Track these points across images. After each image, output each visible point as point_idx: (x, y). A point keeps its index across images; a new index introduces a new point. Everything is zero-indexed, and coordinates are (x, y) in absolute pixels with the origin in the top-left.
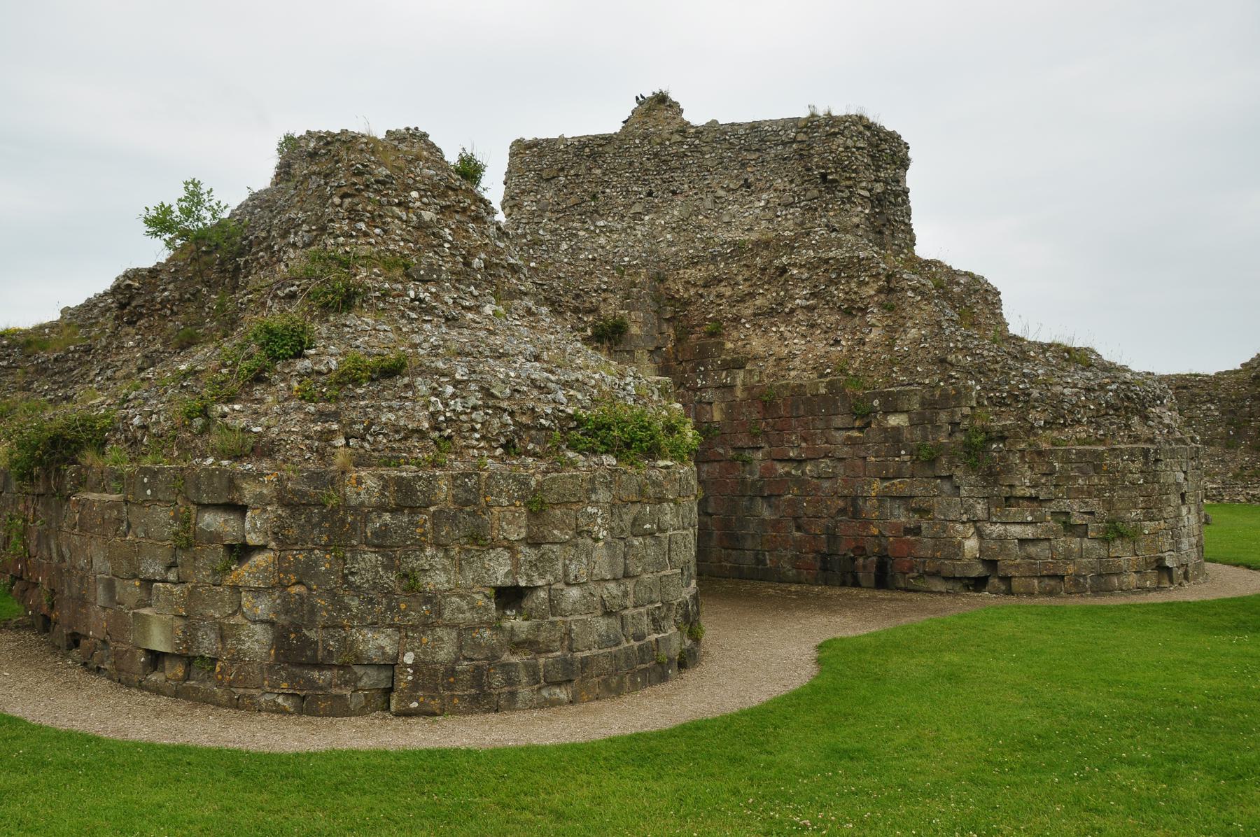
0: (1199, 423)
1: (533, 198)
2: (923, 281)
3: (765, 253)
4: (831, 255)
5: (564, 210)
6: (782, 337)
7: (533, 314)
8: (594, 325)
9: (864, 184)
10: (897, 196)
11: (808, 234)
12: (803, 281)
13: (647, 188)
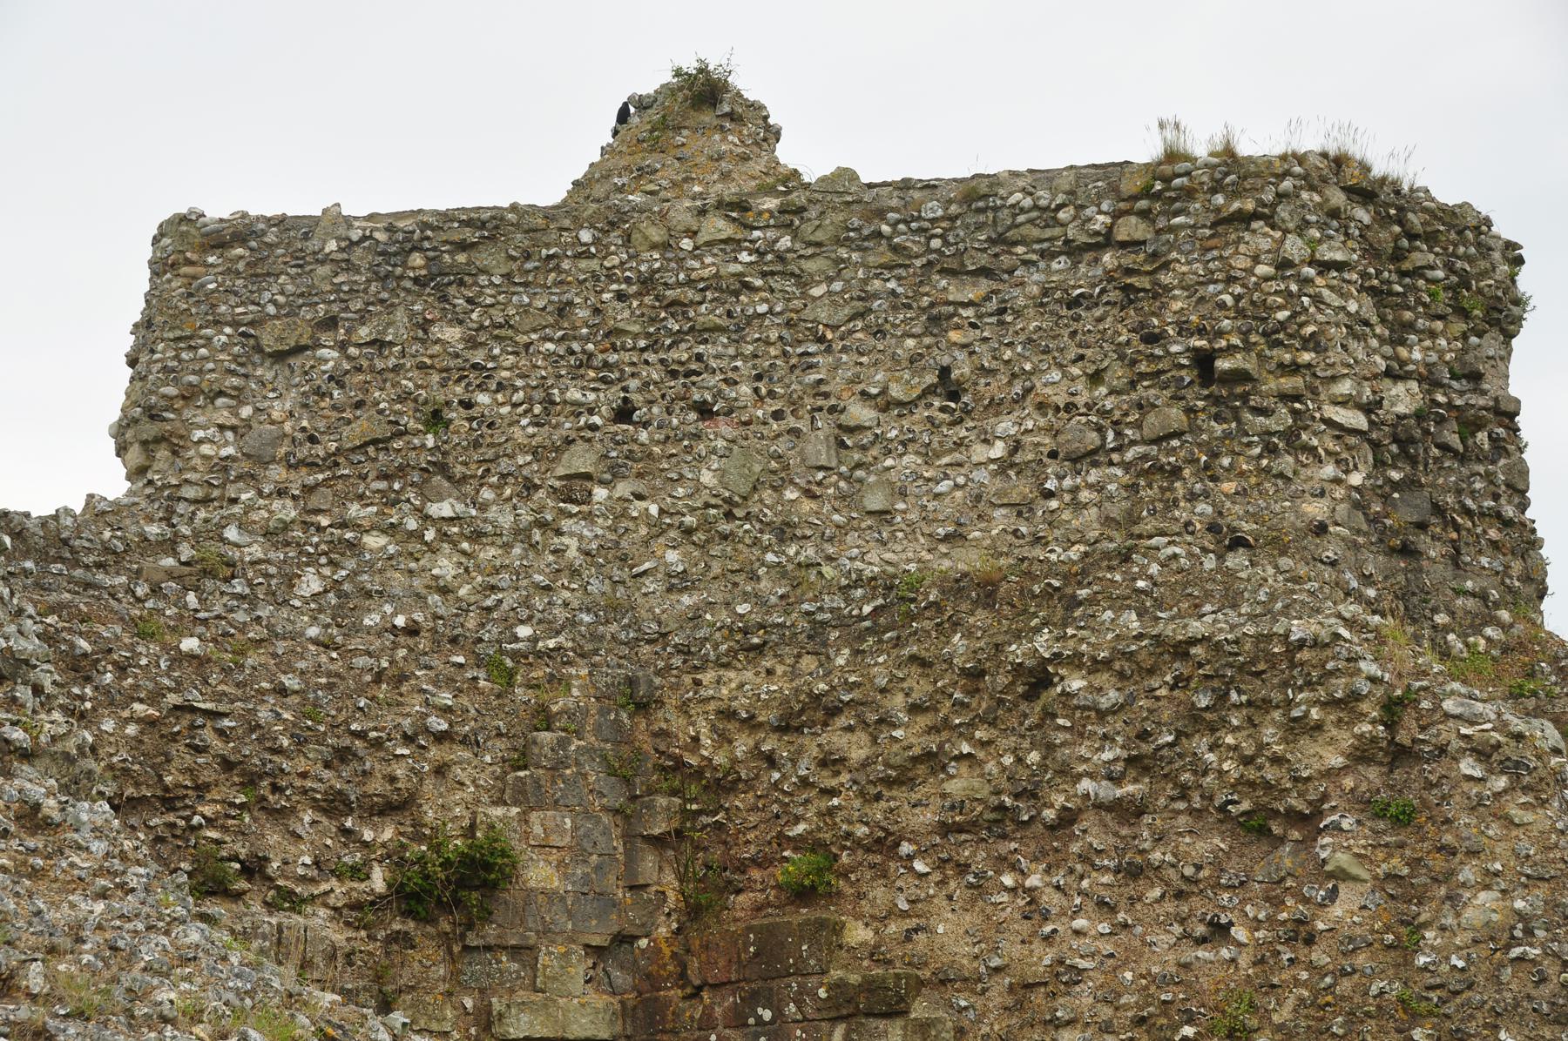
1: (224, 417)
2: (1517, 725)
3: (980, 618)
4: (1196, 627)
5: (331, 461)
6: (1034, 910)
7: (48, 825)
8: (395, 857)
9: (1345, 387)
10: (1470, 425)
11: (1126, 558)
12: (1102, 715)
13: (614, 394)
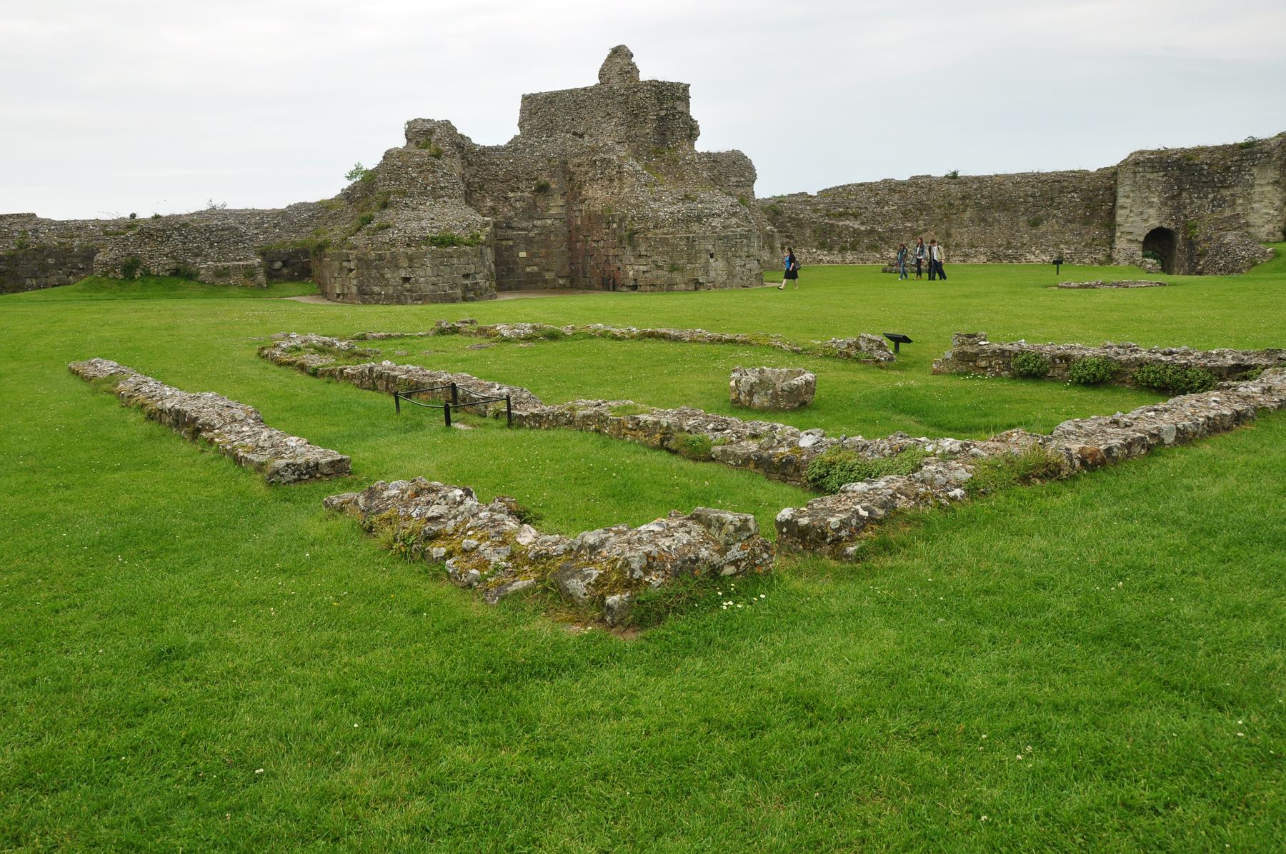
0: (1065, 207)
